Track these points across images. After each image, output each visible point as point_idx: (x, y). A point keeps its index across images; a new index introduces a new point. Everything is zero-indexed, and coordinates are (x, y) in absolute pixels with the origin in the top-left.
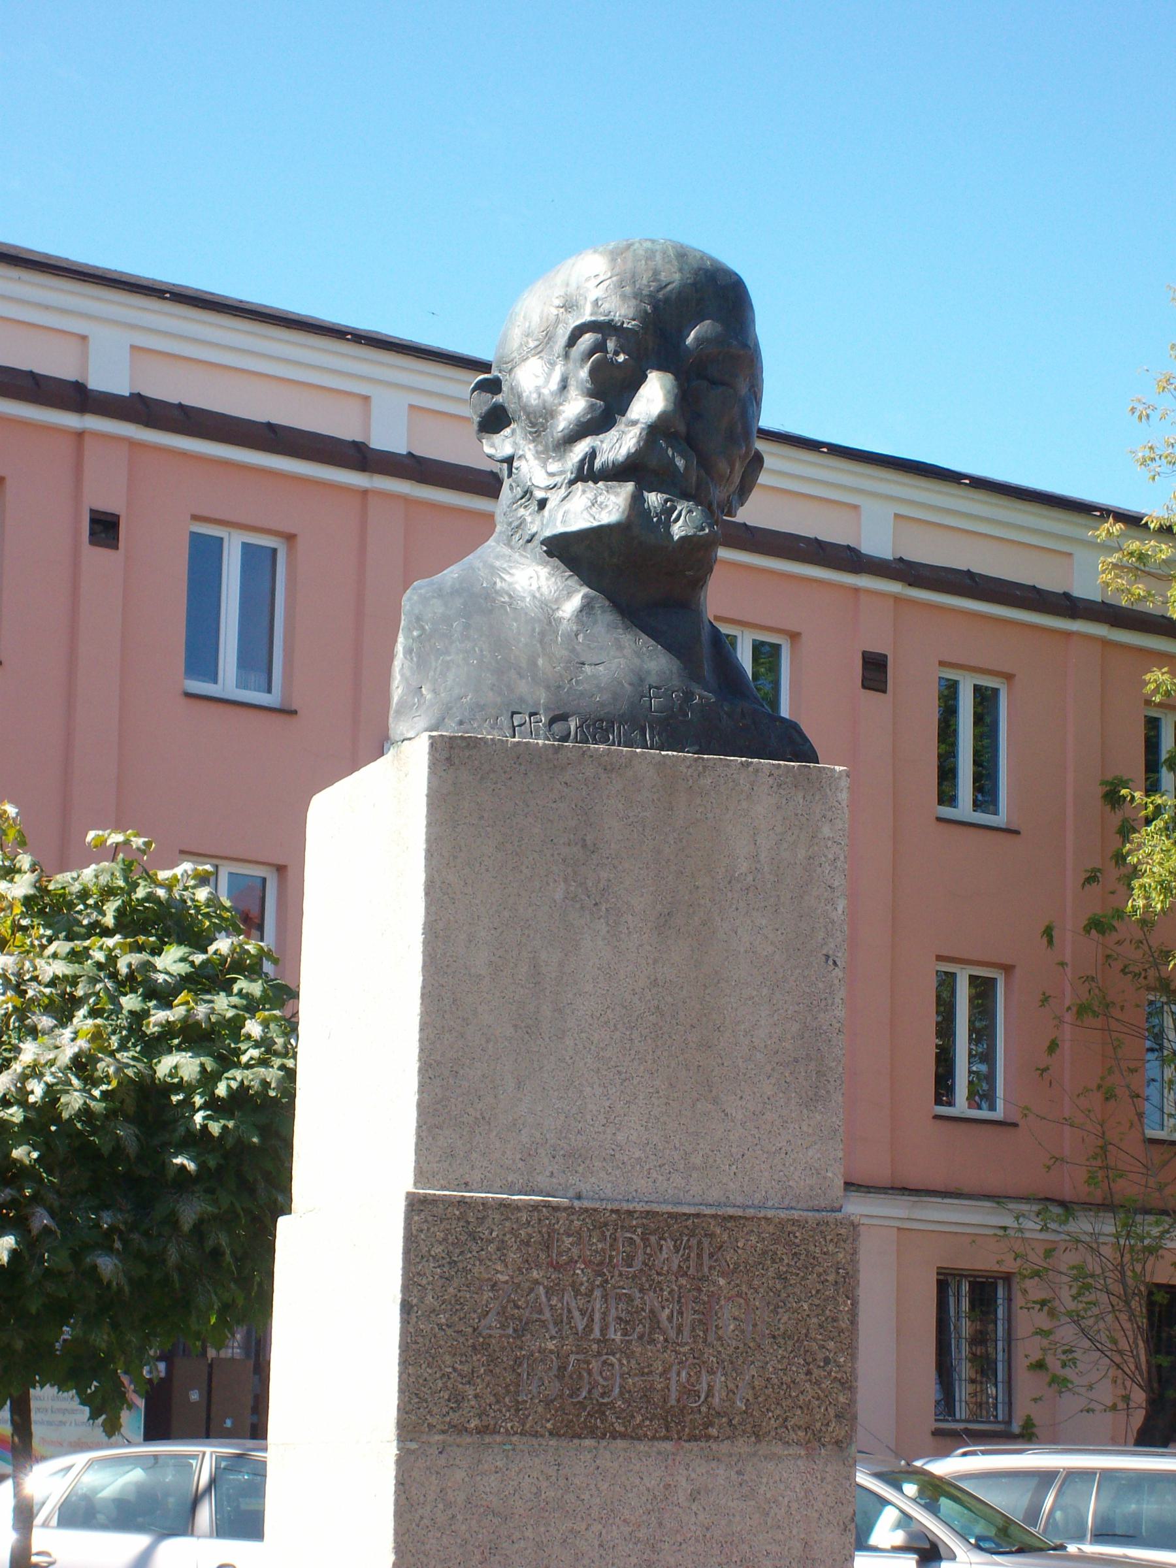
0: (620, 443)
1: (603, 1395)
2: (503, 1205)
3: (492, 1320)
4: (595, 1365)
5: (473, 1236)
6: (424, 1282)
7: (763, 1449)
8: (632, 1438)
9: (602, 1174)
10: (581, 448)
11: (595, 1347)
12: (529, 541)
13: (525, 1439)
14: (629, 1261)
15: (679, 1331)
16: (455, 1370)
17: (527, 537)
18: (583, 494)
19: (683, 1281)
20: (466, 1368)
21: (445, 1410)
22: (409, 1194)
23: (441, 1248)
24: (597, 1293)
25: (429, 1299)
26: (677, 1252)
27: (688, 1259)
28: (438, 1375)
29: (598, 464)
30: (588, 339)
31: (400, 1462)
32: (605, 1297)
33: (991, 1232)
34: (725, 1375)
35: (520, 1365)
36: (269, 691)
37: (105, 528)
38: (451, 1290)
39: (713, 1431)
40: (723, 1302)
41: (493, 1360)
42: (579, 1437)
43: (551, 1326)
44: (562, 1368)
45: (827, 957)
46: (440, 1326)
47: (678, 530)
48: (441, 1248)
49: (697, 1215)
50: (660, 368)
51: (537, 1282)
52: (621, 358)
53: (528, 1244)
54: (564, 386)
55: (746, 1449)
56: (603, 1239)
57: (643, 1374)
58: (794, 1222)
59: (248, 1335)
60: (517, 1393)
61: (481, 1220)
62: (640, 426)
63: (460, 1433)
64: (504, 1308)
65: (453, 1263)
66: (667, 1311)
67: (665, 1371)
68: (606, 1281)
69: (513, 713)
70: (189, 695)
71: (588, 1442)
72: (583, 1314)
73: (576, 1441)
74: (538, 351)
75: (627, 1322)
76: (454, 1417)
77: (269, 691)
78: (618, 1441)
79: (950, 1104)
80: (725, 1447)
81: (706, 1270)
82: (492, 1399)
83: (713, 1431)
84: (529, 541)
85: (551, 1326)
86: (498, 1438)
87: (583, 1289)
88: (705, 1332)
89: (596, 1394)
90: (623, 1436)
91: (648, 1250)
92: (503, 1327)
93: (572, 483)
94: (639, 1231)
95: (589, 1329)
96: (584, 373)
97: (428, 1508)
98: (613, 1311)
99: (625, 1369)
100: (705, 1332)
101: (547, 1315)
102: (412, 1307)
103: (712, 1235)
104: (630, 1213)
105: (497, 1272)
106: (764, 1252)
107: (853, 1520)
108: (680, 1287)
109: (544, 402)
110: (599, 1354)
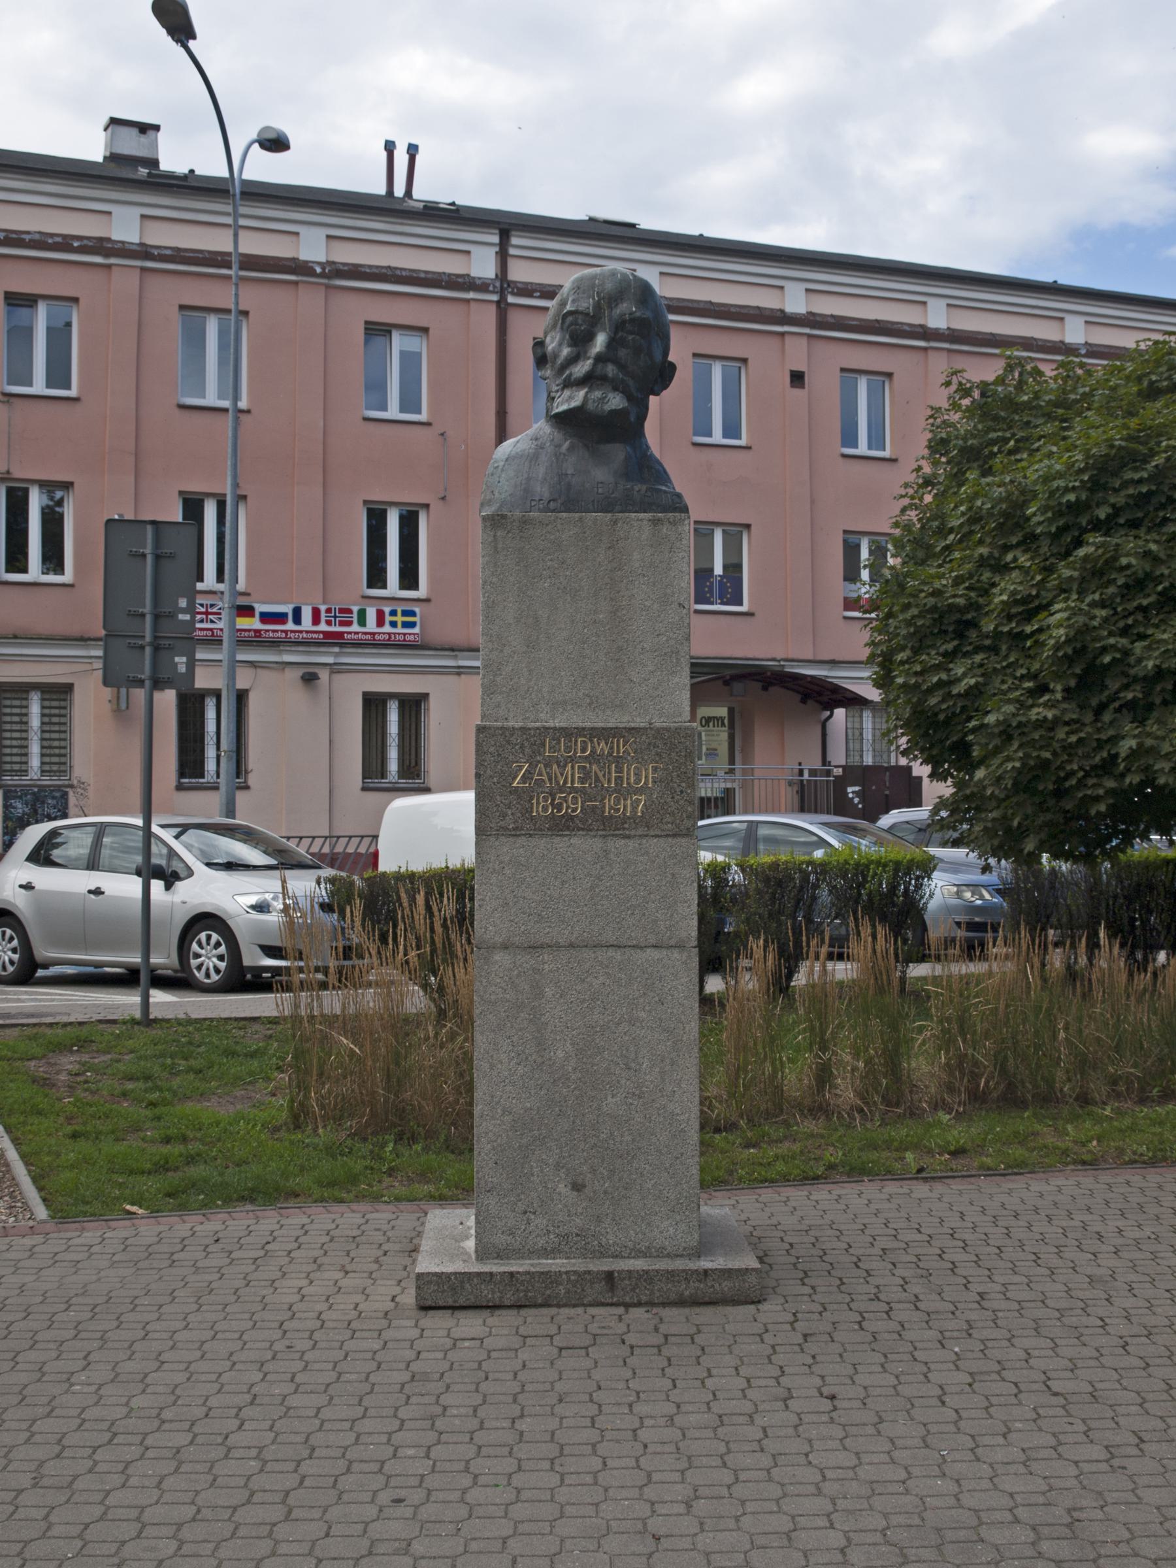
0: (581, 369)
5: (508, 742)
25: (488, 771)
33: (293, 1275)
41: (519, 797)
58: (664, 729)
59: (959, 645)
62: (1128, 1177)
65: (499, 755)
79: (25, 570)
83: (626, 826)
90: (583, 829)
95: (565, 782)
104: (584, 729)
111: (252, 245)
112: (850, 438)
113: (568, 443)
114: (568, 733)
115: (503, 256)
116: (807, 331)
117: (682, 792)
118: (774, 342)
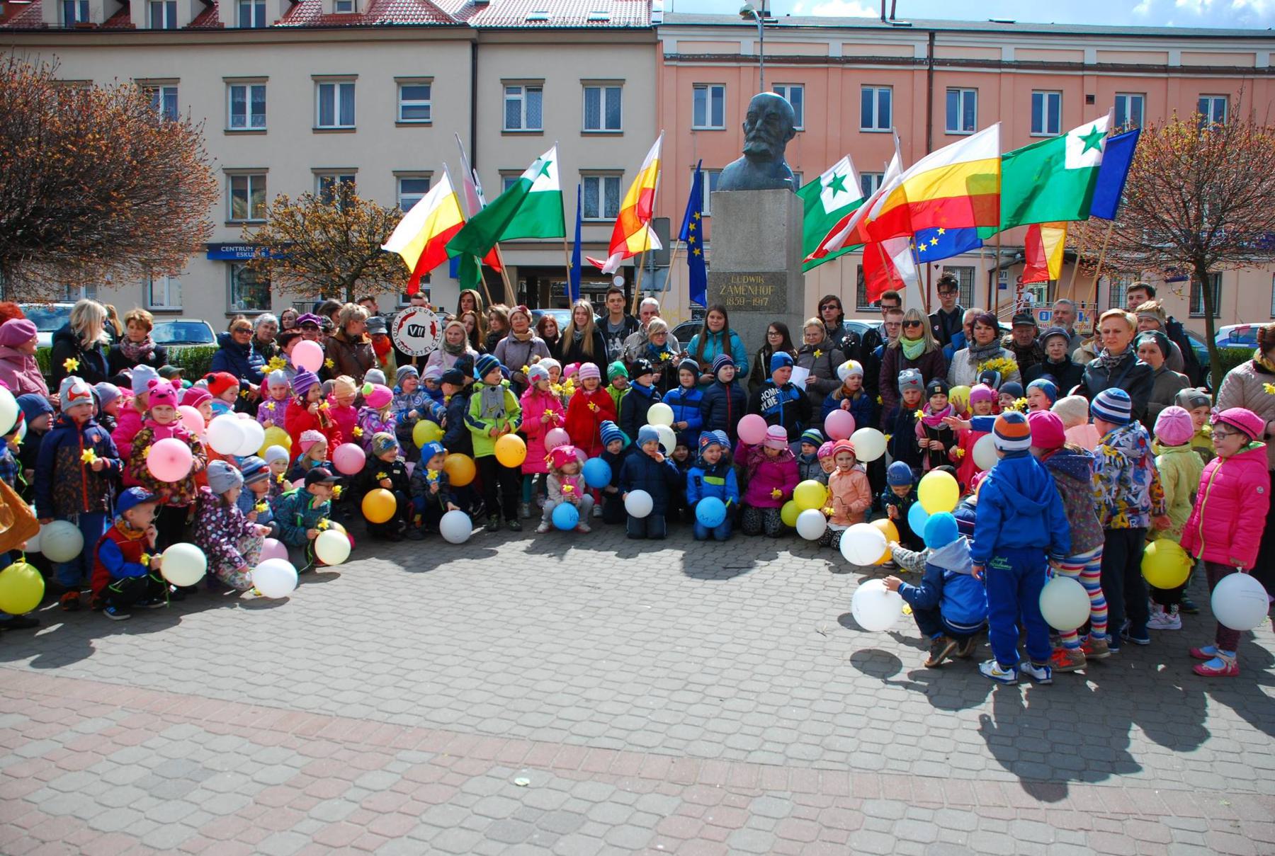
111: (769, 51)
114: (740, 274)
115: (931, 46)
118: (996, 78)
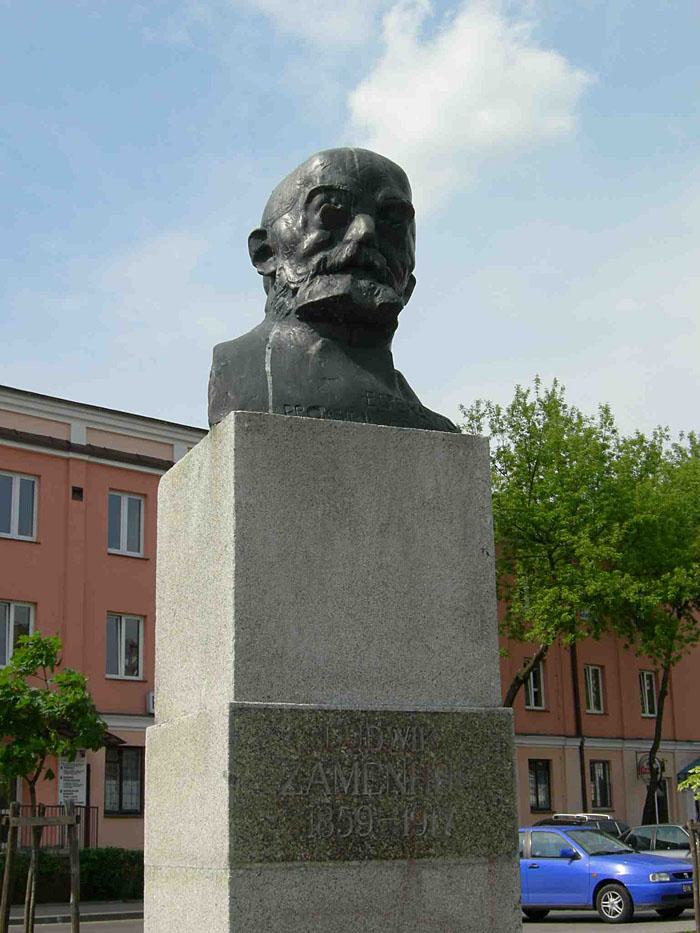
0: (343, 252)
1: (362, 832)
2: (293, 710)
3: (289, 785)
4: (357, 812)
5: (275, 731)
6: (244, 762)
7: (463, 860)
8: (381, 858)
9: (355, 689)
10: (316, 260)
11: (355, 800)
12: (287, 314)
13: (313, 864)
14: (374, 744)
15: (408, 787)
16: (266, 819)
17: (286, 312)
18: (319, 284)
19: (408, 755)
20: (273, 819)
21: (262, 846)
22: (231, 704)
23: (254, 739)
24: (356, 764)
26: (404, 736)
27: (411, 740)
28: (256, 823)
29: (328, 264)
30: (317, 199)
31: (232, 883)
32: (361, 767)
34: (437, 814)
35: (309, 814)
36: (139, 551)
37: (78, 493)
38: (261, 766)
39: (432, 851)
40: (434, 767)
41: (291, 812)
42: (348, 859)
43: (327, 787)
44: (336, 815)
45: (483, 549)
46: (255, 791)
47: (378, 301)
48: (254, 739)
49: (415, 712)
50: (363, 212)
51: (316, 759)
52: (339, 206)
53: (310, 735)
54: (306, 223)
55: (453, 861)
56: (357, 730)
57: (387, 816)
58: (475, 715)
60: (307, 833)
61: (279, 720)
63: (271, 861)
64: (296, 778)
66: (400, 775)
67: (401, 813)
68: (361, 757)
69: (285, 405)
70: (109, 554)
71: (355, 863)
72: (347, 778)
73: (346, 862)
74: (288, 211)
75: (375, 783)
76: (267, 851)
77: (139, 551)
78: (373, 861)
80: (440, 860)
81: (423, 747)
82: (291, 838)
83: (432, 851)
84: (287, 314)
85: (327, 787)
86: (296, 864)
87: (346, 763)
88: (424, 787)
89: (357, 831)
90: (376, 857)
91: (386, 736)
92: (297, 790)
93: (314, 276)
94: (380, 724)
95: (351, 789)
96: (317, 216)
97: (252, 913)
98: (366, 776)
99: (376, 814)
100: (424, 787)
101: (324, 780)
102: (236, 779)
103: (425, 725)
104: (373, 712)
105: (291, 754)
106: (457, 734)
107: (520, 902)
108: (407, 759)
109: (294, 234)
110: (359, 804)
112: (114, 540)
113: (319, 343)
116: (86, 458)
117: (498, 801)
